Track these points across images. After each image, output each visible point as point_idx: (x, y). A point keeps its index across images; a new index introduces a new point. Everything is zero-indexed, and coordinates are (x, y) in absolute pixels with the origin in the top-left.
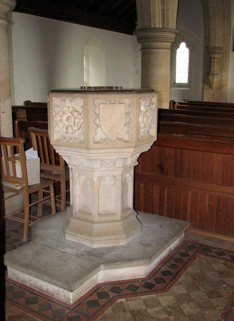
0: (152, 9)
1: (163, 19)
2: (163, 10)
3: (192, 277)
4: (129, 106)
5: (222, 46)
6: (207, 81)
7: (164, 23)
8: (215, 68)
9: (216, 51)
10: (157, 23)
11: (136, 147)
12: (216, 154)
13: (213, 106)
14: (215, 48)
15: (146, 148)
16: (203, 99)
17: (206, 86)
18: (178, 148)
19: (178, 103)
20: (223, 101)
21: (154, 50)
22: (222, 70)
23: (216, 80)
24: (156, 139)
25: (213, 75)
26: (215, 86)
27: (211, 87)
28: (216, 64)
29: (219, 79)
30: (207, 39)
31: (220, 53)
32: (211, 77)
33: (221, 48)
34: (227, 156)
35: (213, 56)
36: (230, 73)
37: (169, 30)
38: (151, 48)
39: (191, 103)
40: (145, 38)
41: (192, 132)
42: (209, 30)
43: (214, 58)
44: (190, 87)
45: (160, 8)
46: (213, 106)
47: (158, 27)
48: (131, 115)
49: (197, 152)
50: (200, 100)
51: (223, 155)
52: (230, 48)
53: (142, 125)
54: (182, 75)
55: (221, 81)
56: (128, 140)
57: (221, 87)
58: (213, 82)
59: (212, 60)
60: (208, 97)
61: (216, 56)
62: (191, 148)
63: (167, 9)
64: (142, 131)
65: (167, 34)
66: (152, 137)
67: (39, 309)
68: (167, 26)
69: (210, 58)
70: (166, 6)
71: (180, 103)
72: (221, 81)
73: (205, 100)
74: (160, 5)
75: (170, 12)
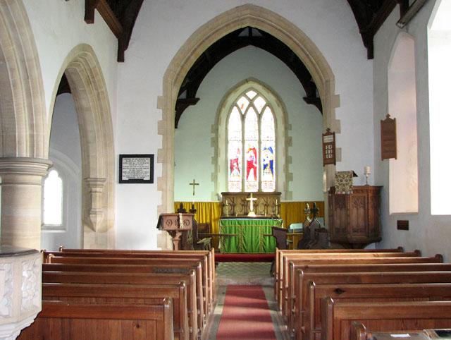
0: (17, 134)
1: (32, 146)
2: (32, 136)
3: (345, 228)
4: (9, 272)
5: (105, 177)
6: (87, 221)
7: (32, 151)
8: (97, 204)
9: (99, 183)
10: (24, 151)
11: (18, 322)
12: (113, 321)
13: (111, 256)
14: (96, 179)
15: (28, 322)
16: (82, 245)
17: (86, 228)
18: (65, 318)
19: (52, 253)
20: (109, 248)
21: (14, 185)
22: (105, 206)
23: (99, 220)
24: (41, 310)
25: (95, 213)
26: (98, 227)
27: (93, 229)
28: (98, 198)
29: (103, 219)
30: (86, 168)
31: (103, 185)
32: (92, 216)
33: (104, 180)
34: (127, 322)
35: (94, 189)
36: (116, 211)
37: (40, 161)
38: (16, 183)
39: (67, 253)
40: (8, 170)
41: (79, 295)
42: (88, 156)
43: (96, 192)
44: (64, 229)
45: (28, 133)
46: (111, 256)
47: (25, 156)
48: (12, 283)
49: (89, 321)
50: (79, 247)
51: (120, 321)
52: (114, 178)
53: (24, 294)
54: (54, 216)
55: (105, 221)
56: (7, 314)
57: (105, 230)
58: (96, 223)
59: (93, 194)
60: (90, 243)
61: (98, 189)
62: (82, 316)
63: (38, 136)
64: (24, 301)
65: (36, 166)
66: (37, 307)
67: (368, 236)
68: (37, 155)
69: (91, 192)
70: (37, 131)
71: (55, 254)
72: (105, 221)
73: (87, 247)
74: (28, 129)
75: (41, 139)
